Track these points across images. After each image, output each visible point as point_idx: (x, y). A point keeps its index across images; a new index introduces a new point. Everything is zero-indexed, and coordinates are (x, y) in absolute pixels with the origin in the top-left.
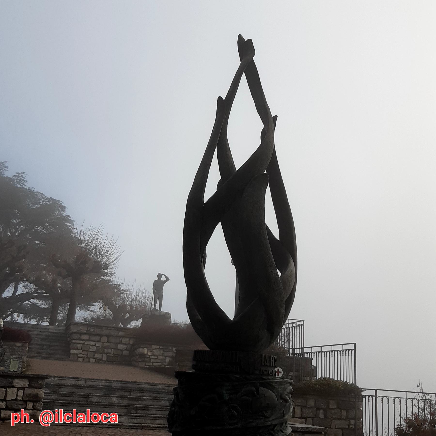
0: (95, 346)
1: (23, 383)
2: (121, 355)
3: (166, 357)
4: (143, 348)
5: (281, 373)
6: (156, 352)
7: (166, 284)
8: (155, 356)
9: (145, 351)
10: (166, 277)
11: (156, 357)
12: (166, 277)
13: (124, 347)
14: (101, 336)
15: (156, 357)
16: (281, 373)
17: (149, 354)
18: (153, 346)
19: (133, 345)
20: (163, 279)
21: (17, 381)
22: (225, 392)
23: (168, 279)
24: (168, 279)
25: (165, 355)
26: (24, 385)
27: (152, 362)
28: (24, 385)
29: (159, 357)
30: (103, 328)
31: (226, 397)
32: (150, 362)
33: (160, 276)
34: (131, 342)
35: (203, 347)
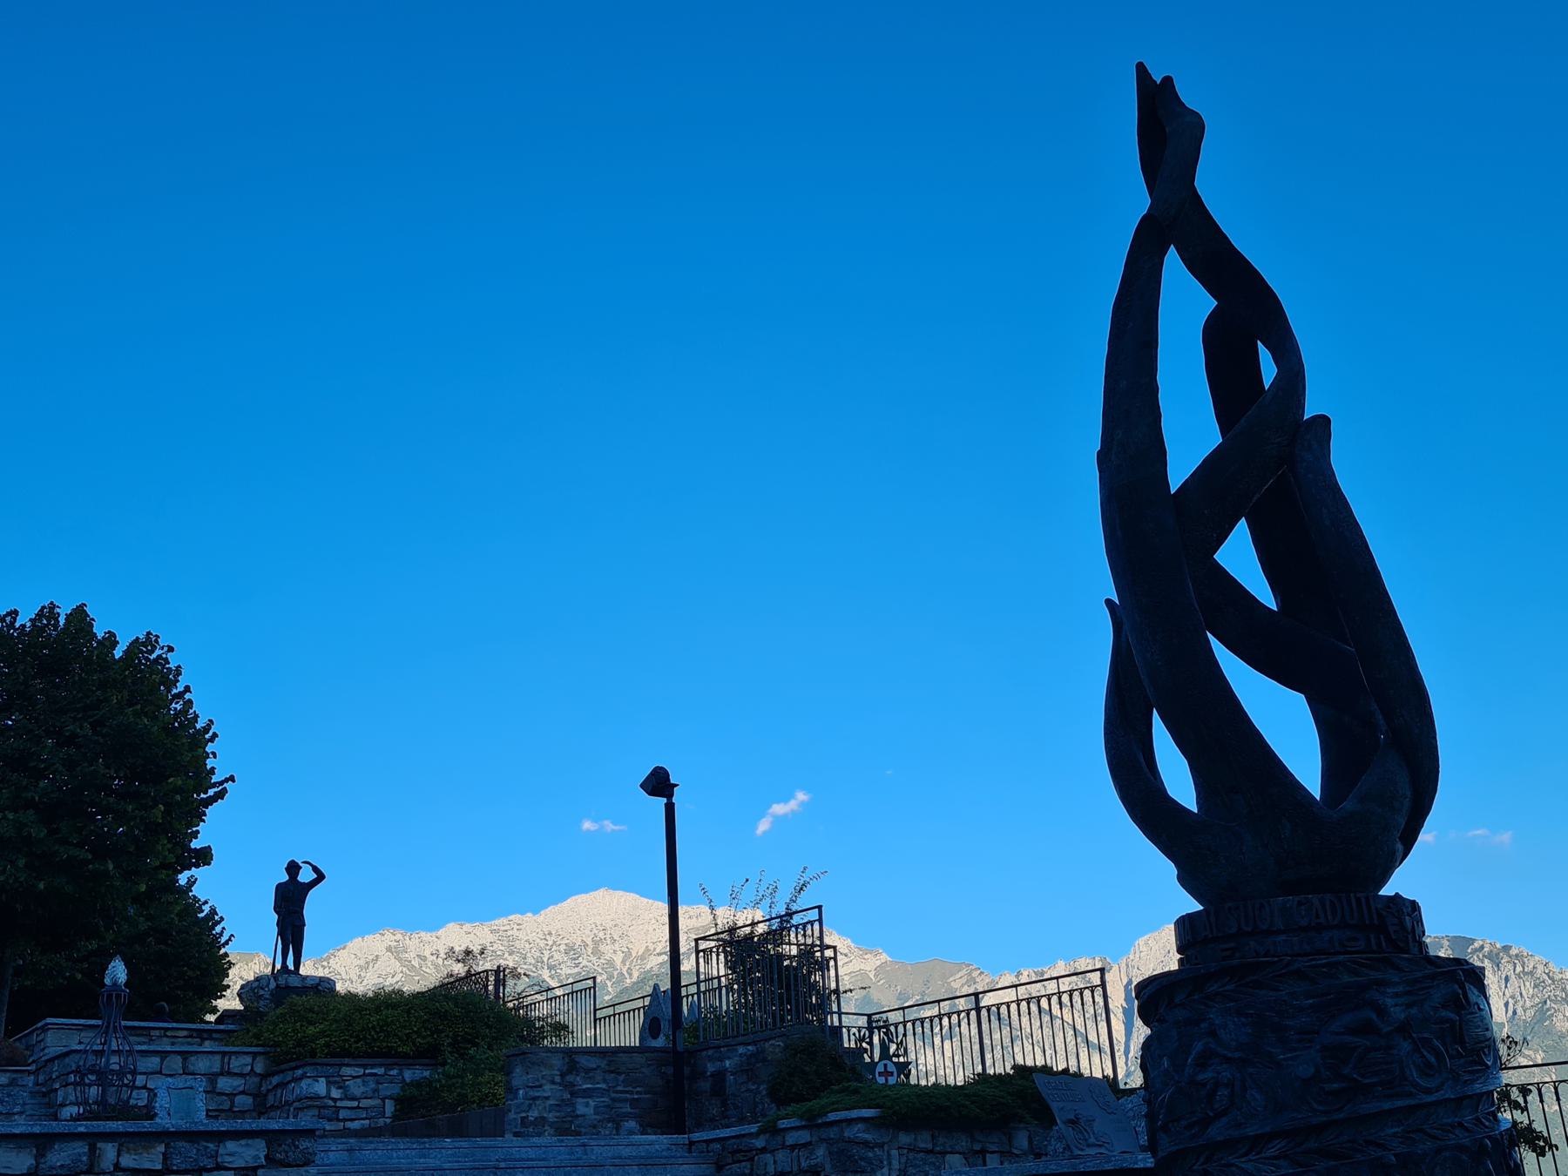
0: (145, 1087)
1: (252, 1152)
2: (230, 1110)
3: (383, 1100)
4: (315, 1078)
5: (892, 1074)
6: (356, 1088)
7: (312, 895)
8: (353, 1099)
9: (320, 1087)
10: (315, 869)
11: (355, 1104)
12: (315, 869)
13: (238, 1082)
14: (164, 1055)
15: (355, 1104)
16: (892, 1074)
17: (335, 1093)
18: (347, 1071)
19: (264, 1077)
20: (306, 876)
21: (231, 1146)
22: (1389, 1001)
23: (320, 877)
24: (320, 877)
25: (382, 1094)
26: (257, 1157)
27: (345, 1120)
28: (257, 1157)
29: (364, 1103)
30: (153, 1033)
31: (1398, 1014)
32: (339, 1120)
33: (293, 868)
34: (259, 1069)
35: (1195, 906)
